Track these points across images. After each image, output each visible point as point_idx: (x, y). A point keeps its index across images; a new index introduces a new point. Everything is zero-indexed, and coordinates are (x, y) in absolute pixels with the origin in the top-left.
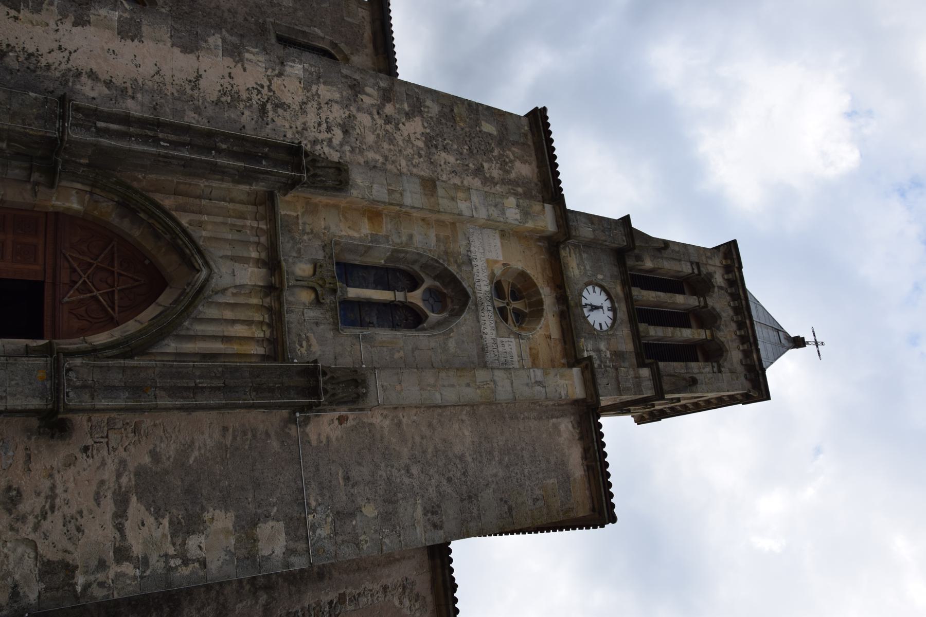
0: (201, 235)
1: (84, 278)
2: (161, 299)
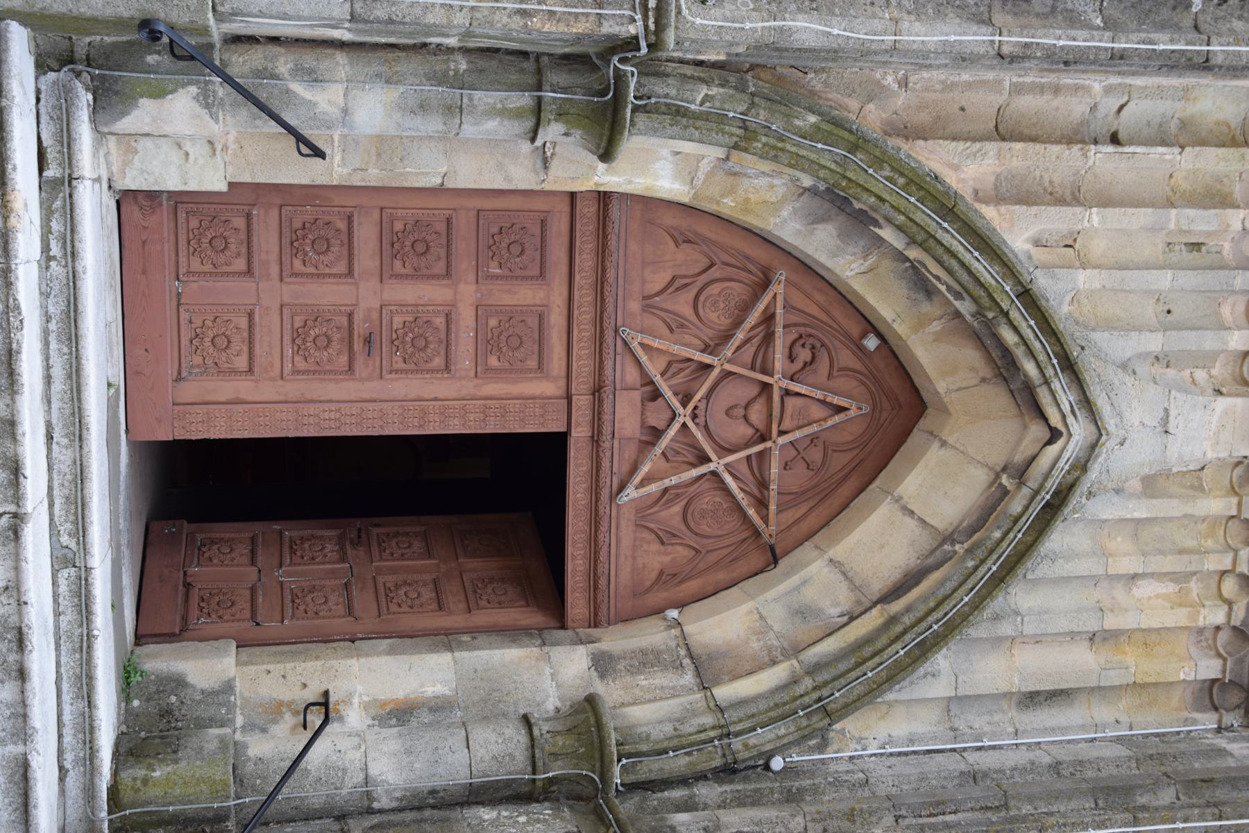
1: (684, 415)
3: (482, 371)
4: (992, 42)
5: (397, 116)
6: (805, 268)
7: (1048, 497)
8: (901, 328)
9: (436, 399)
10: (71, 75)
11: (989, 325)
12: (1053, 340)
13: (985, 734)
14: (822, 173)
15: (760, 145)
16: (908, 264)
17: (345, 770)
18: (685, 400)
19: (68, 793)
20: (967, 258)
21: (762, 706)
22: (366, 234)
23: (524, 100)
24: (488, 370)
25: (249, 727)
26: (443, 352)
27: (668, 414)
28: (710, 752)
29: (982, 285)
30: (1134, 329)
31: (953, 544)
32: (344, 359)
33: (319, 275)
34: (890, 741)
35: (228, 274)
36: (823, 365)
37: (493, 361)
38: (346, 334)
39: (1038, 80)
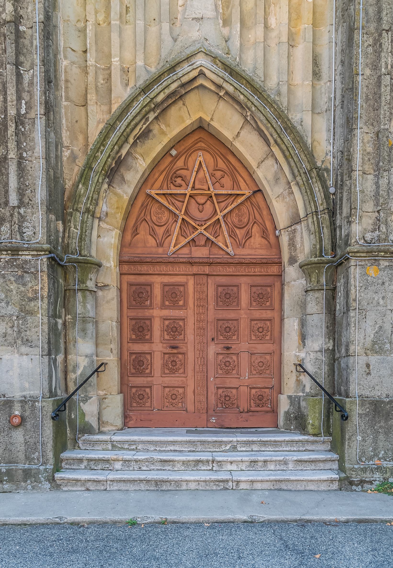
0: (144, 67)
1: (201, 230)
2: (228, 134)
3: (185, 306)
4: (40, 118)
5: (87, 339)
6: (145, 181)
7: (227, 74)
8: (166, 140)
9: (194, 324)
10: (79, 440)
11: (157, 105)
12: (163, 77)
13: (329, 96)
14: (100, 181)
15: (91, 206)
16: (138, 141)
17: (317, 359)
18: (195, 229)
19: (314, 449)
20: (130, 118)
21: (306, 198)
22: (138, 348)
23: (79, 295)
24: (184, 305)
25: (303, 391)
26: (178, 321)
27: (201, 236)
28: (323, 219)
29: (141, 111)
30: (160, 37)
31: (248, 116)
32: (180, 356)
33: (151, 364)
34: (328, 140)
35: (151, 394)
36: (183, 172)
37: (181, 303)
38: (171, 355)
39: (63, 90)
